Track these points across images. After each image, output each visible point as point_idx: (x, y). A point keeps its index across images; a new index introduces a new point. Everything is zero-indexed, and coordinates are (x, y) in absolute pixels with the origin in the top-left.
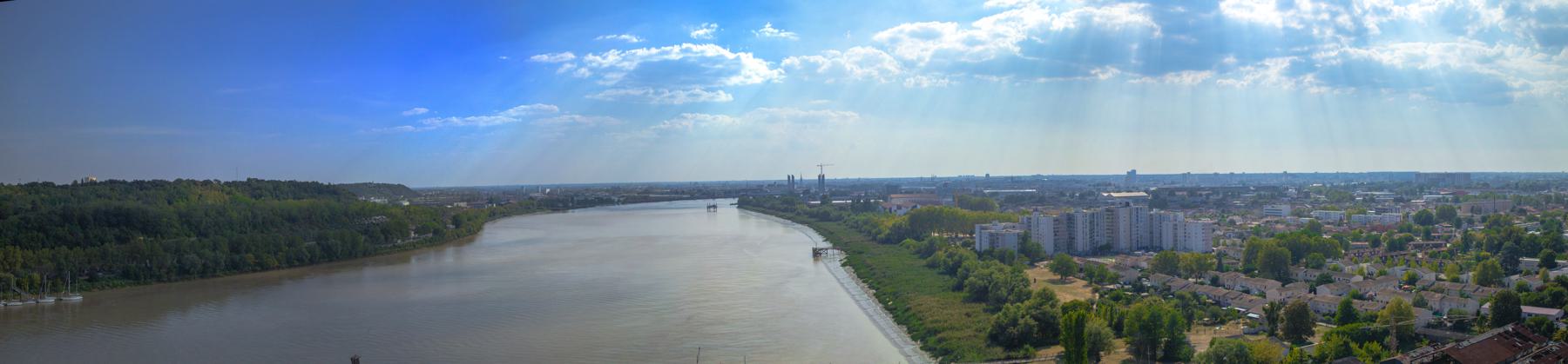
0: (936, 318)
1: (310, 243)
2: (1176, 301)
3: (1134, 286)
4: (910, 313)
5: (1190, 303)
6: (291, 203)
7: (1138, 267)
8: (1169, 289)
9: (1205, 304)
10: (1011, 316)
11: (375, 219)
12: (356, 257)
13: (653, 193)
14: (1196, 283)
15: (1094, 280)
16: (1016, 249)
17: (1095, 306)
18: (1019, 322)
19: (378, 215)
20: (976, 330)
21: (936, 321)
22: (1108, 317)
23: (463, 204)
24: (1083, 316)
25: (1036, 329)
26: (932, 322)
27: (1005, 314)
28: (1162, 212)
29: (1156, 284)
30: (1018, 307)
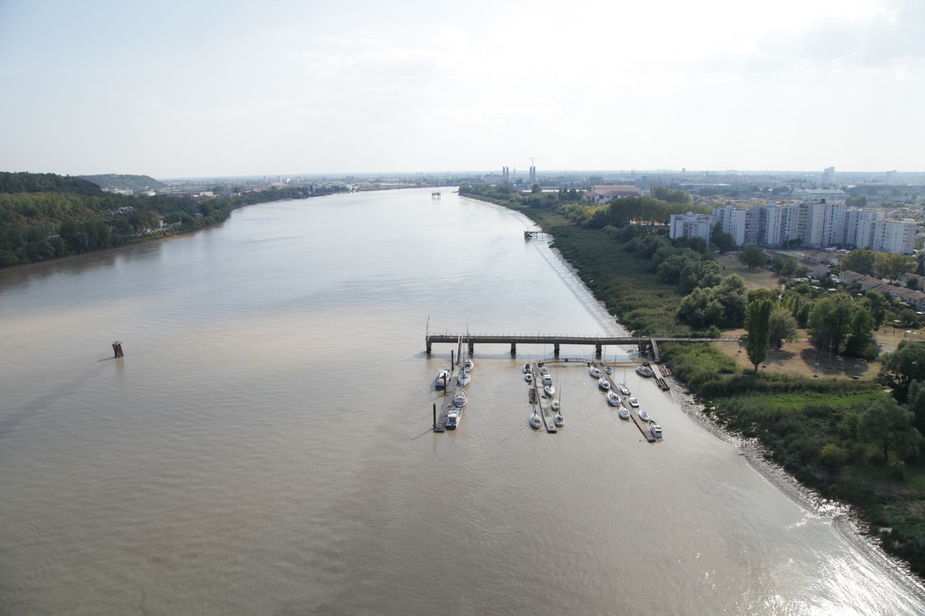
0: (631, 296)
1: (54, 236)
2: (866, 299)
3: (822, 281)
4: (609, 291)
5: (882, 303)
6: (27, 198)
7: (828, 263)
8: (859, 286)
9: (898, 305)
10: (700, 299)
11: (122, 210)
12: (105, 247)
13: (383, 182)
14: (890, 284)
15: (781, 272)
16: (708, 238)
17: (780, 297)
18: (708, 305)
19: (124, 206)
20: (667, 309)
21: (632, 299)
22: (793, 307)
23: (210, 194)
24: (769, 304)
25: (722, 312)
26: (628, 300)
27: (694, 296)
28: (861, 210)
29: (845, 281)
30: (707, 292)
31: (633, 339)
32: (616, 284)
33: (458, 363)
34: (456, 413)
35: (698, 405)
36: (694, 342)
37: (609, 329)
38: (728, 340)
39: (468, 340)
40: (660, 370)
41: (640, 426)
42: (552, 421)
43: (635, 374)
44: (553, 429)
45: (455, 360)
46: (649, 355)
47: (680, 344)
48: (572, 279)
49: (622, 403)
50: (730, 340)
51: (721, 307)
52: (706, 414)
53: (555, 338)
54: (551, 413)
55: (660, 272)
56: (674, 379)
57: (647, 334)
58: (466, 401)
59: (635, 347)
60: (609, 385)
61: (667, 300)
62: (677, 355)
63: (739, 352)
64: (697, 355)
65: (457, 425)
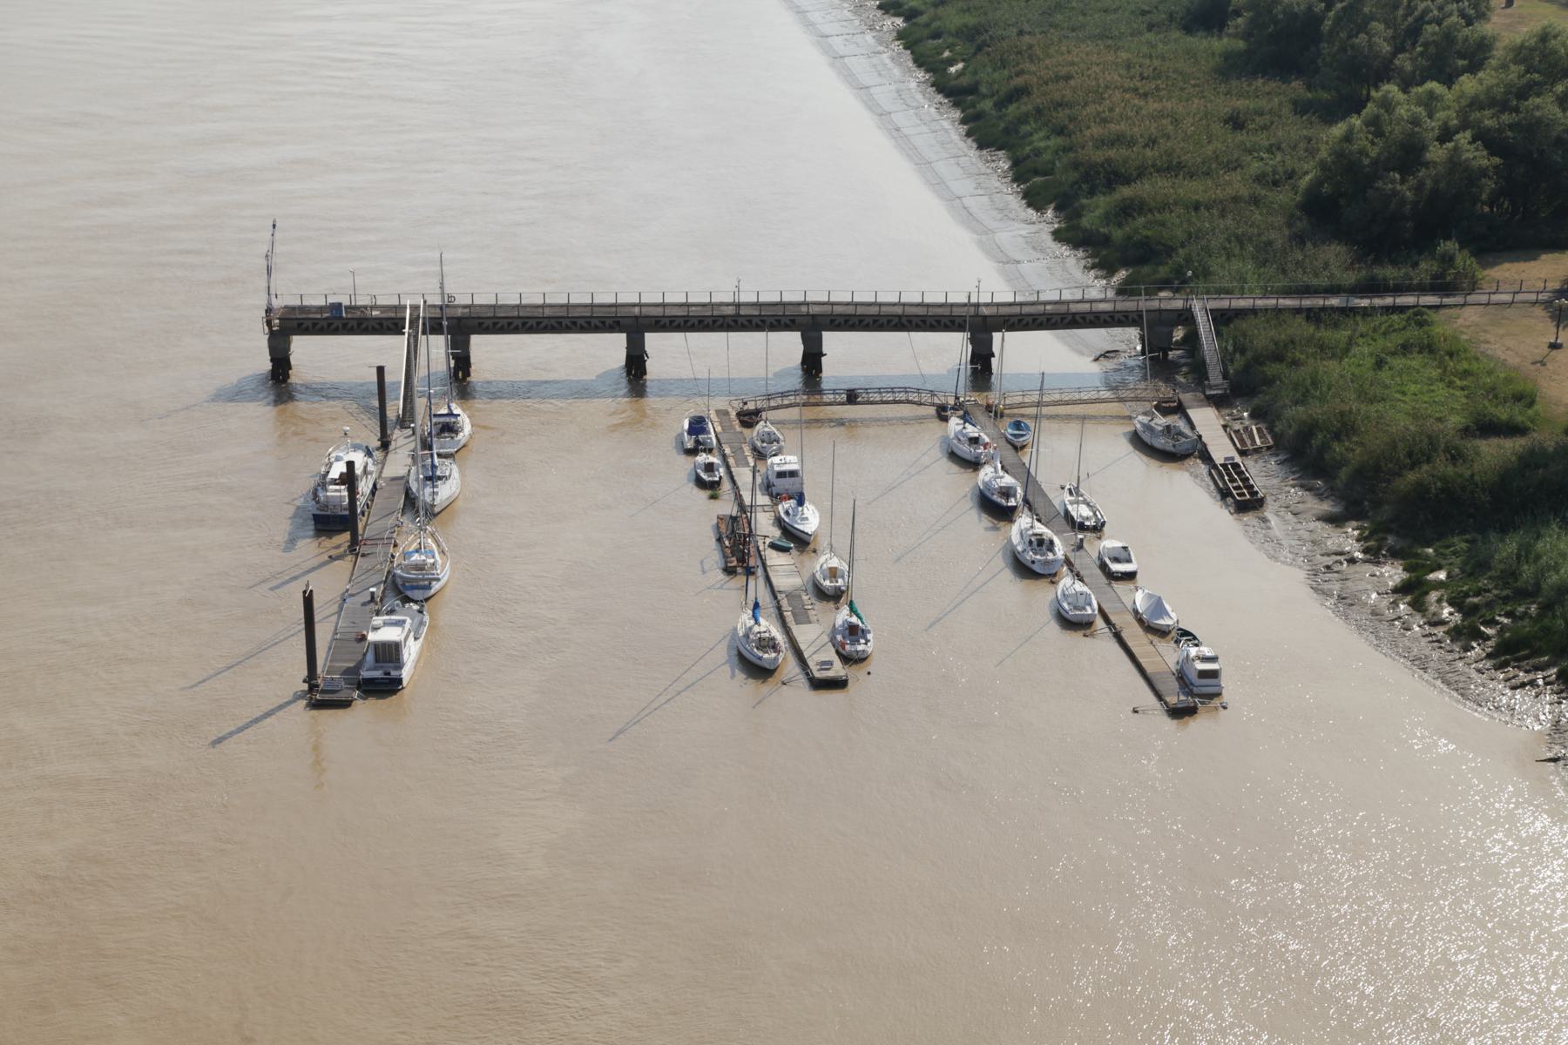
10: (1396, 131)
18: (1429, 156)
20: (1260, 179)
21: (1118, 140)
25: (1489, 185)
26: (1101, 143)
27: (1374, 124)
30: (1430, 101)
31: (1121, 306)
32: (1057, 78)
33: (405, 420)
34: (400, 623)
35: (1378, 563)
36: (1366, 312)
37: (1025, 267)
38: (1507, 298)
39: (445, 323)
40: (1225, 427)
41: (1135, 650)
42: (826, 638)
43: (1125, 447)
44: (830, 674)
45: (395, 407)
46: (1184, 369)
47: (1308, 318)
48: (875, 60)
49: (1068, 562)
50: (1519, 297)
51: (1485, 162)
52: (1408, 598)
53: (804, 309)
54: (818, 609)
55: (1240, 20)
56: (1281, 463)
57: (1176, 282)
58: (444, 573)
59: (1128, 339)
60: (1020, 492)
61: (1263, 140)
62: (1295, 363)
63: (1554, 346)
64: (1380, 364)
65: (406, 674)
